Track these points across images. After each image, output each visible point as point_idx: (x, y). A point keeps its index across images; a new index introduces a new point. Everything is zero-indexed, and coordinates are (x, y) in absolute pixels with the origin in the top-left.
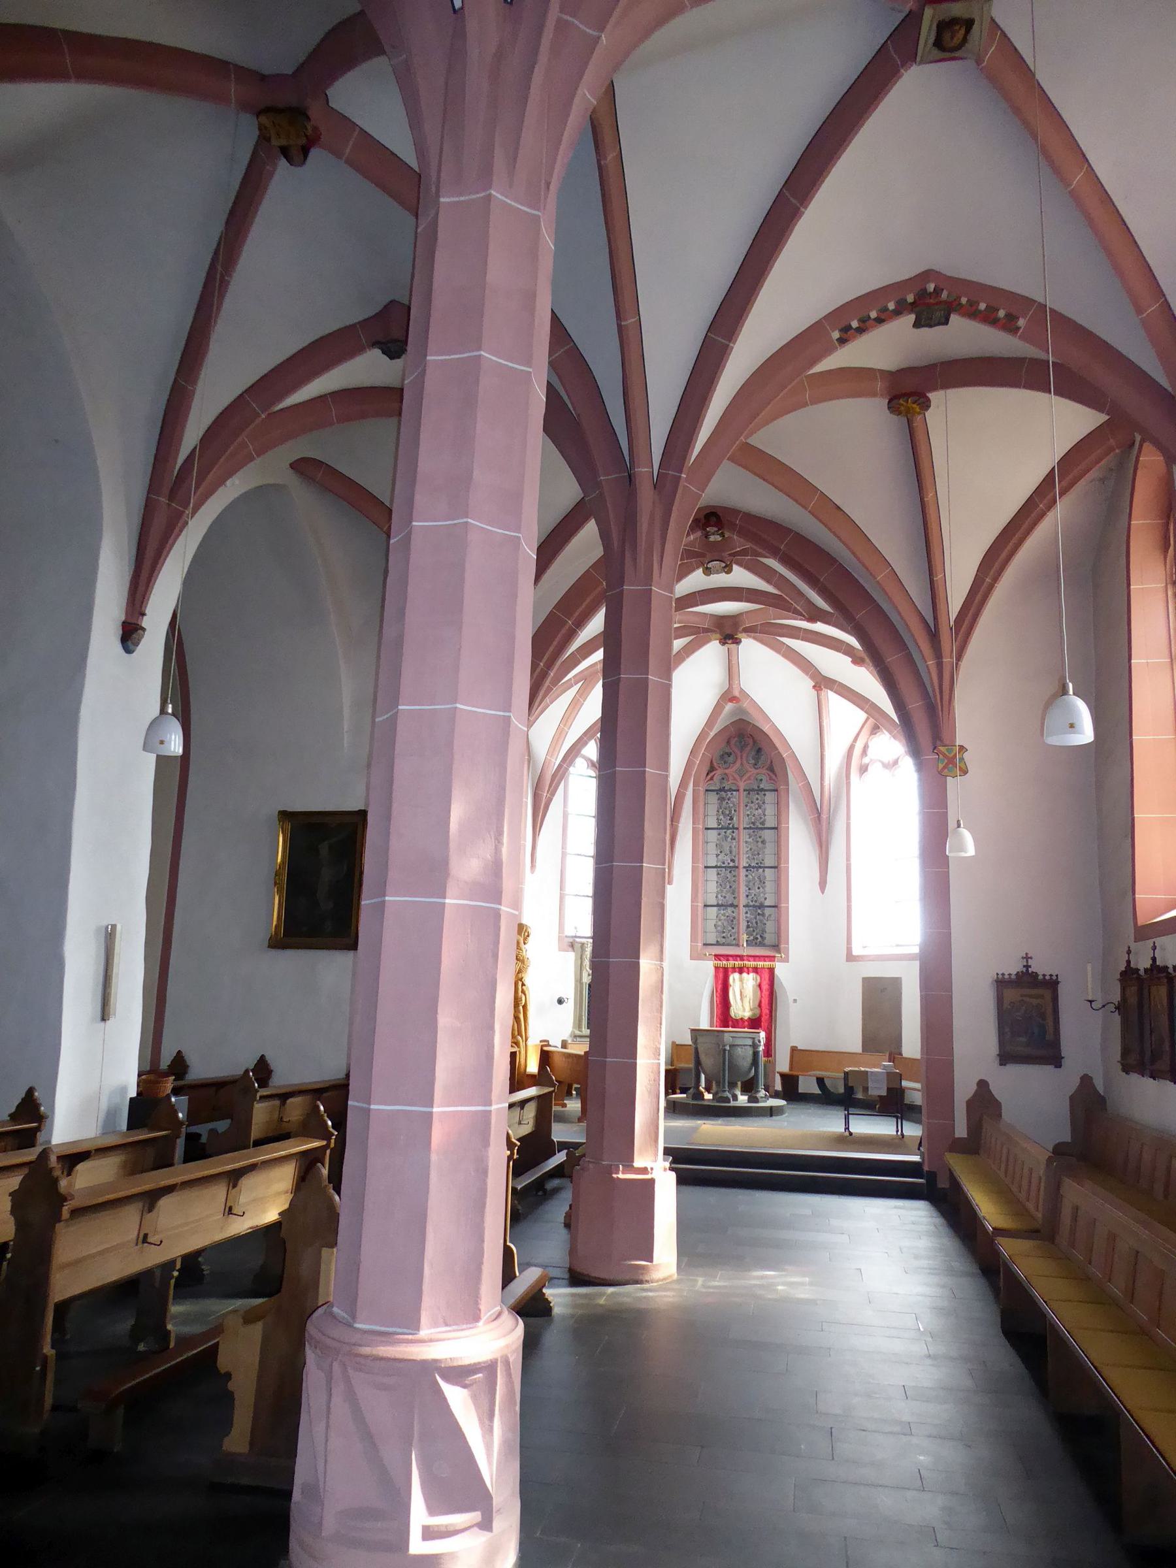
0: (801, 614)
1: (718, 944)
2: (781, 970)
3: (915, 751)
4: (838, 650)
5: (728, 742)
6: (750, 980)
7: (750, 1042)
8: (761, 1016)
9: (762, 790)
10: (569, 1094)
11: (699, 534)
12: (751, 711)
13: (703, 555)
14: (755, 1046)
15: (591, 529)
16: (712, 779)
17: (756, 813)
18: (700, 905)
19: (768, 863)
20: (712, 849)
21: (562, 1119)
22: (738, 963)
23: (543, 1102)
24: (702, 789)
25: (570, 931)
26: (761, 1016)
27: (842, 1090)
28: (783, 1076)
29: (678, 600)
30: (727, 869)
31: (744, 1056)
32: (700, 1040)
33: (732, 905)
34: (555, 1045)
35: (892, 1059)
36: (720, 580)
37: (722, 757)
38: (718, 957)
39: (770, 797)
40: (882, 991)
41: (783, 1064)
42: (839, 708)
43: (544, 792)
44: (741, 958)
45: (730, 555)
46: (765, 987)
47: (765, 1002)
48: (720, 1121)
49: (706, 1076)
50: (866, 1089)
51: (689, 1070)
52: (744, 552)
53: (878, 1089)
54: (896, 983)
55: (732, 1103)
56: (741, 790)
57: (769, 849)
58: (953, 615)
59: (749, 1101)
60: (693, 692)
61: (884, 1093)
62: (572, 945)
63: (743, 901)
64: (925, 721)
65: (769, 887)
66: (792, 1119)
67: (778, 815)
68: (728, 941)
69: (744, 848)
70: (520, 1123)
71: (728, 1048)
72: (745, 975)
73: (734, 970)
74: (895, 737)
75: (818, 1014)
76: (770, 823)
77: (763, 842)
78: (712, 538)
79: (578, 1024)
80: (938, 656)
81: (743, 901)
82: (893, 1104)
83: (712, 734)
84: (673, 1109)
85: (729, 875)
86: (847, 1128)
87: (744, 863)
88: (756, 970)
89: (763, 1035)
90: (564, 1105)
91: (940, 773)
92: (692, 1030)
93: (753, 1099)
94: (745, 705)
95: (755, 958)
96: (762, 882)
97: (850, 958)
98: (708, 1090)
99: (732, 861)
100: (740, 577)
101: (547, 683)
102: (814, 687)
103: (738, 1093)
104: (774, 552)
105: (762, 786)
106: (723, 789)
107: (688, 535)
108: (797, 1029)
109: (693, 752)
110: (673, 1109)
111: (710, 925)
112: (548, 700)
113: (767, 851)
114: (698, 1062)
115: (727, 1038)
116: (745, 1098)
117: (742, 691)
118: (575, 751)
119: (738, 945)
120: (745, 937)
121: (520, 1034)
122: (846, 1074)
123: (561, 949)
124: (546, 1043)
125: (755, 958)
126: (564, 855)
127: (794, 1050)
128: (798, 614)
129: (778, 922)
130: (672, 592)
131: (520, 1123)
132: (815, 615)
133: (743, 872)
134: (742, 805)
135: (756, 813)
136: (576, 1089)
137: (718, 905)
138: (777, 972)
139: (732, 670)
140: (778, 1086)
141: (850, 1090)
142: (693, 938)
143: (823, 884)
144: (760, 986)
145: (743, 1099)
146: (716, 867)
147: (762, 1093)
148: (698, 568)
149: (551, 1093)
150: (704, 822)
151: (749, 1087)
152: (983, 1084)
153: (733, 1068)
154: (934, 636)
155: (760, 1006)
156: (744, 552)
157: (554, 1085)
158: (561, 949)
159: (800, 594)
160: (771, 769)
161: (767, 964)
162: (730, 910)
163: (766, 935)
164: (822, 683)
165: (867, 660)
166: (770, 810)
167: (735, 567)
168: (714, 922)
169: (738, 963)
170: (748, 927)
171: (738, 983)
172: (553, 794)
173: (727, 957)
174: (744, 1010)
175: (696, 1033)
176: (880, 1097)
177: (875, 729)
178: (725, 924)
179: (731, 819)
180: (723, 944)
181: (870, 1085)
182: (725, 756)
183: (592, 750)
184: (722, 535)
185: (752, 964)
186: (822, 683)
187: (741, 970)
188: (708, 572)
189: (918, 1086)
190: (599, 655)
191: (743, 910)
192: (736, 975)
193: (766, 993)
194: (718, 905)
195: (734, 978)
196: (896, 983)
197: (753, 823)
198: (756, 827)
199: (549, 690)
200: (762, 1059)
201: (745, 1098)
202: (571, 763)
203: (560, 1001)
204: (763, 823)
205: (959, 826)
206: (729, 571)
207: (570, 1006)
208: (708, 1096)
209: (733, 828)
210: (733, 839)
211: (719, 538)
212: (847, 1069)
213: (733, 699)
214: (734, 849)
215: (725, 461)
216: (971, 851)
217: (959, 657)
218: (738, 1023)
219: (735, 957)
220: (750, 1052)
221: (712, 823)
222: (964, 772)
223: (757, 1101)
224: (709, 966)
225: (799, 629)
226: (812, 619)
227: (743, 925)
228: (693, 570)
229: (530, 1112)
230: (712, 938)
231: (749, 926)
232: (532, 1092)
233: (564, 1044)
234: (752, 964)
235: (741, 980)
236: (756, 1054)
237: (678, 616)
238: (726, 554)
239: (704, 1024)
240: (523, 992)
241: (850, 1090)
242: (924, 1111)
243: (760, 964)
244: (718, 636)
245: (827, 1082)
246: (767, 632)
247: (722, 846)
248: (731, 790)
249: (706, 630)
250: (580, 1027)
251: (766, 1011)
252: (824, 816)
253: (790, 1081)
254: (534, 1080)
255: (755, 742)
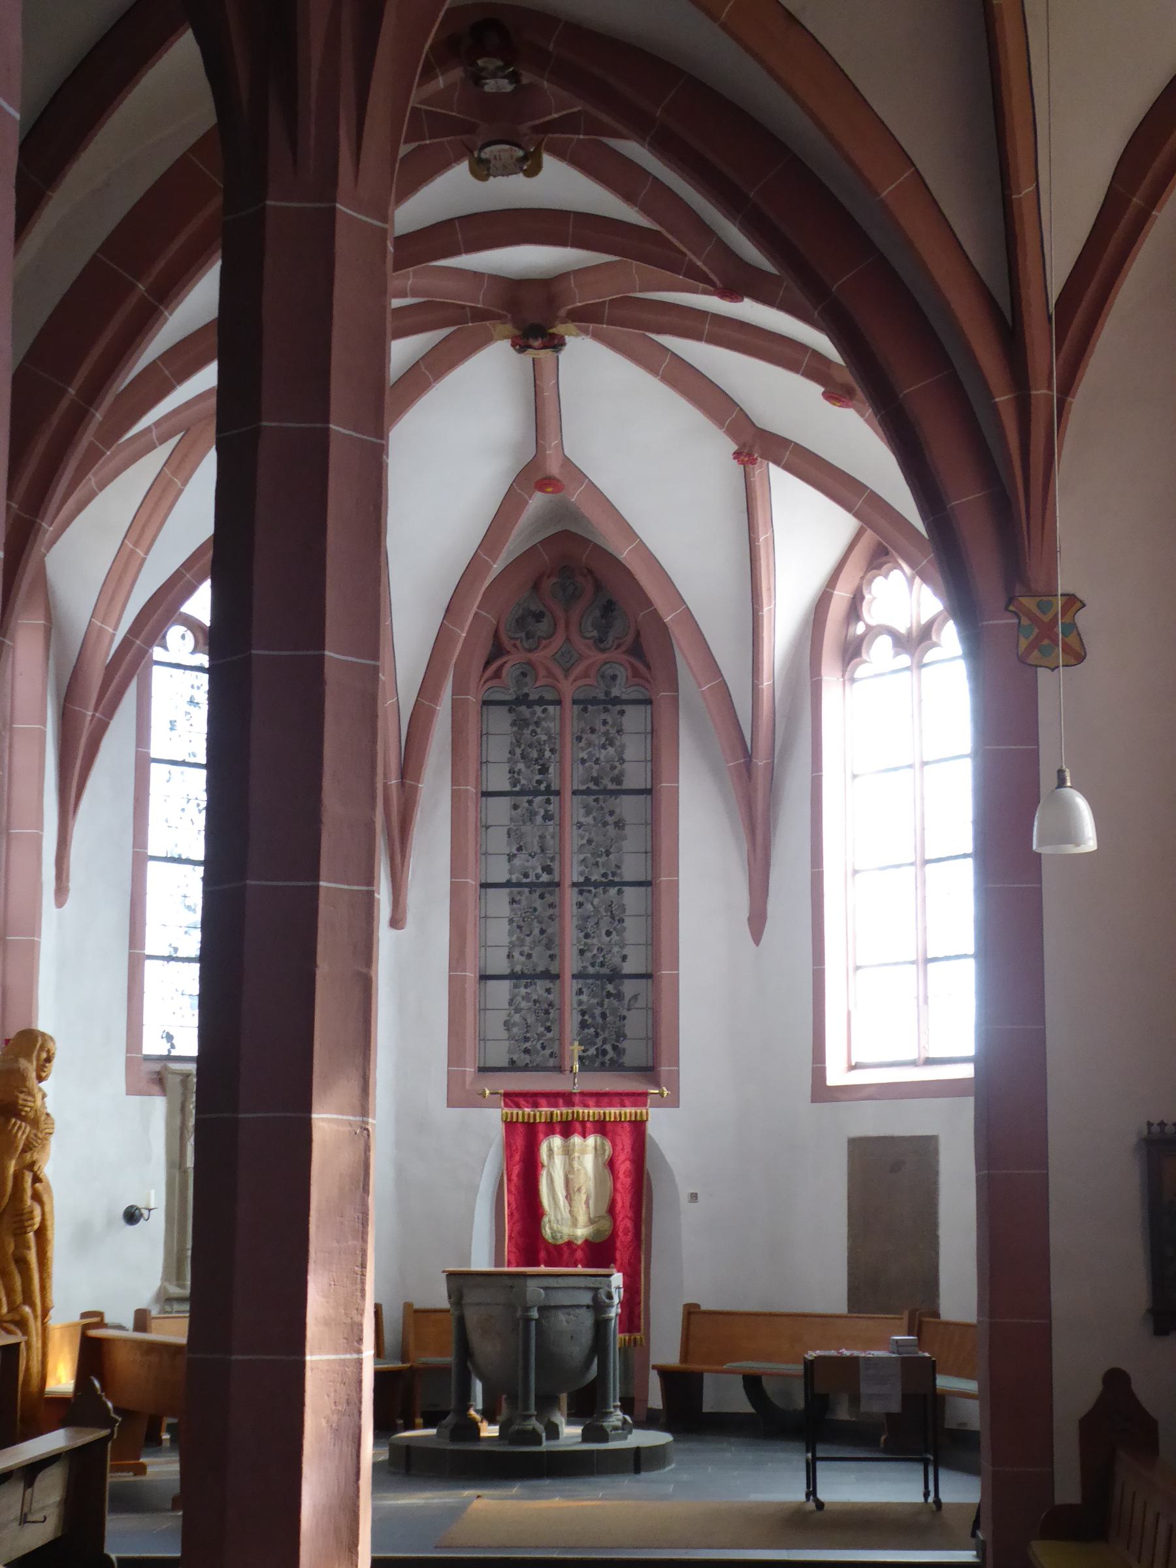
0: (706, 279)
1: (513, 1067)
2: (661, 1125)
3: (965, 605)
4: (792, 365)
5: (536, 586)
6: (587, 1151)
7: (586, 1298)
8: (613, 1235)
9: (616, 701)
10: (152, 1441)
11: (457, 74)
12: (591, 511)
13: (471, 129)
14: (599, 1307)
15: (184, 52)
16: (497, 674)
17: (602, 755)
18: (471, 975)
19: (628, 874)
20: (498, 841)
21: (134, 1502)
22: (560, 1112)
23: (83, 1467)
24: (472, 700)
25: (153, 1045)
26: (613, 1235)
27: (800, 1403)
28: (665, 1374)
29: (401, 241)
30: (536, 890)
31: (572, 1330)
32: (470, 1297)
33: (547, 975)
34: (120, 1315)
35: (916, 1327)
36: (512, 190)
37: (521, 622)
38: (512, 1098)
39: (634, 718)
40: (896, 1167)
41: (665, 1346)
42: (793, 502)
43: (93, 700)
44: (567, 1098)
45: (536, 129)
46: (624, 1166)
47: (624, 1201)
48: (516, 1489)
49: (487, 1382)
50: (855, 1400)
51: (443, 1370)
52: (568, 124)
53: (882, 1400)
54: (923, 1150)
55: (546, 1445)
56: (568, 702)
57: (633, 840)
58: (1055, 288)
59: (586, 1437)
60: (442, 475)
61: (895, 1407)
62: (154, 1076)
63: (571, 963)
64: (979, 513)
65: (634, 930)
66: (685, 1477)
67: (654, 759)
68: (538, 1060)
69: (573, 839)
70: (24, 1520)
71: (535, 1314)
72: (576, 1139)
73: (550, 1128)
74: (936, 594)
75: (750, 1235)
76: (635, 777)
77: (619, 824)
78: (491, 86)
79: (172, 1270)
80: (1020, 379)
81: (571, 963)
82: (916, 1431)
83: (497, 567)
84: (403, 1467)
85: (538, 903)
86: (811, 1492)
87: (573, 873)
88: (602, 1127)
89: (617, 1279)
90: (141, 1470)
91: (1022, 660)
92: (451, 1276)
93: (594, 1433)
94: (575, 497)
95: (600, 1098)
96: (616, 918)
97: (822, 1092)
98: (490, 1415)
99: (547, 869)
100: (560, 184)
101: (87, 438)
102: (737, 455)
103: (560, 1419)
104: (641, 127)
105: (615, 692)
106: (522, 700)
107: (428, 74)
108: (697, 1265)
109: (452, 611)
110: (403, 1467)
111: (495, 1024)
112: (91, 479)
113: (627, 845)
114: (465, 1350)
115: (534, 1291)
116: (577, 1430)
117: (567, 463)
118: (163, 609)
119: (559, 1069)
120: (576, 1049)
121: (28, 1299)
122: (810, 1365)
123: (132, 1090)
124: (94, 1319)
125: (600, 1098)
126: (140, 859)
127: (691, 1312)
128: (699, 280)
129: (654, 1012)
130: (385, 217)
131: (24, 1520)
132: (738, 282)
133: (571, 896)
134: (568, 738)
135: (602, 755)
136: (171, 1429)
137: (512, 976)
138: (651, 1130)
139: (542, 410)
140: (655, 1400)
141: (818, 1403)
142: (455, 1056)
143: (757, 922)
144: (611, 1164)
145: (570, 1433)
146: (508, 884)
147: (617, 1417)
148: (458, 159)
149: (104, 1441)
150: (479, 780)
151: (588, 1406)
152: (1116, 1380)
153: (549, 1360)
154: (1011, 336)
155: (611, 1210)
156: (568, 124)
157: (108, 1422)
158: (132, 1090)
159: (705, 230)
160: (636, 650)
161: (629, 1111)
162: (541, 985)
163: (625, 1044)
164: (757, 445)
165: (859, 392)
166: (634, 748)
167: (548, 160)
168: (503, 1016)
169: (560, 1112)
170: (583, 1025)
171: (558, 1160)
172: (110, 712)
173: (533, 1099)
174: (575, 1224)
175: (460, 1282)
176: (889, 1415)
177: (879, 559)
178: (531, 1019)
179: (544, 770)
180: (526, 1068)
181: (865, 1389)
182: (528, 619)
183: (200, 604)
184: (514, 78)
185: (591, 1112)
186: (757, 445)
187: (567, 1129)
188: (482, 170)
189: (971, 1386)
190: (207, 378)
191: (571, 986)
192: (557, 1141)
193: (625, 1181)
194: (512, 976)
195: (552, 1147)
196: (923, 1150)
197: (596, 781)
198: (603, 789)
199: (92, 457)
200: (617, 1338)
201: (577, 1430)
202: (157, 637)
203: (132, 1216)
204: (618, 780)
205: (1061, 783)
206: (533, 170)
207: (156, 1225)
208: (489, 1431)
209: (549, 791)
210: (547, 817)
211: (506, 86)
212: (811, 1355)
213: (546, 483)
214: (550, 842)
215: (878, 538)
216: (1089, 841)
217: (1068, 386)
218: (561, 1253)
219: (553, 1098)
220: (587, 1319)
221: (499, 779)
222: (1077, 656)
223: (603, 1436)
224: (491, 1121)
225: (702, 314)
226: (731, 292)
227: (572, 1021)
228: (444, 165)
229: (50, 1492)
230: (499, 1054)
231: (583, 1017)
232: (55, 1441)
233: (142, 1320)
234: (591, 1112)
235: (568, 1152)
236: (601, 1326)
237: (409, 278)
238: (525, 127)
239: (481, 1260)
240: (37, 1197)
241: (818, 1403)
242: (985, 1442)
243: (612, 1112)
244: (508, 328)
245: (768, 1386)
246: (629, 324)
247: (521, 837)
248: (541, 701)
249: (480, 315)
250: (179, 1277)
251: (625, 1223)
252: (760, 762)
253: (682, 1386)
254: (63, 1412)
255: (598, 586)
